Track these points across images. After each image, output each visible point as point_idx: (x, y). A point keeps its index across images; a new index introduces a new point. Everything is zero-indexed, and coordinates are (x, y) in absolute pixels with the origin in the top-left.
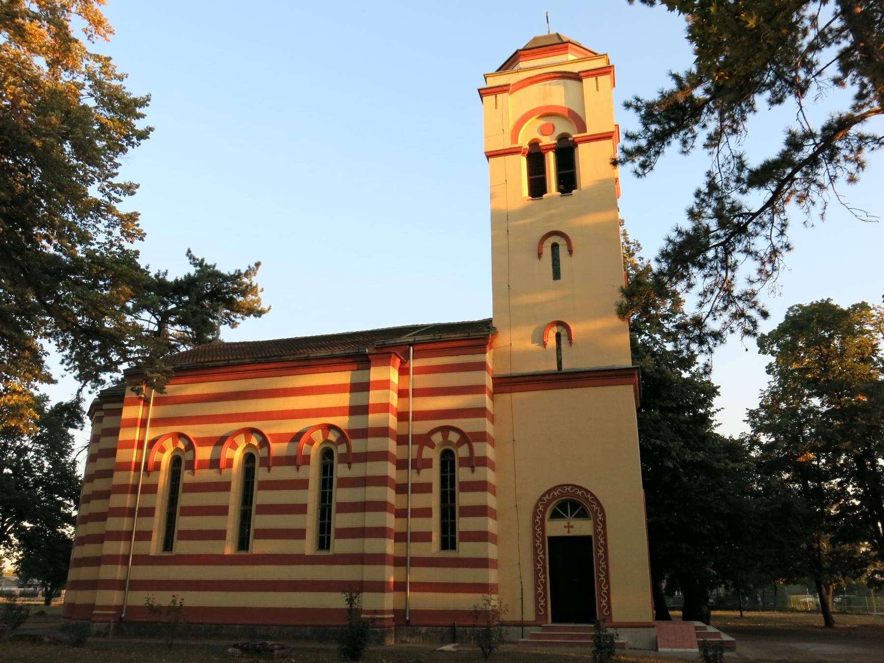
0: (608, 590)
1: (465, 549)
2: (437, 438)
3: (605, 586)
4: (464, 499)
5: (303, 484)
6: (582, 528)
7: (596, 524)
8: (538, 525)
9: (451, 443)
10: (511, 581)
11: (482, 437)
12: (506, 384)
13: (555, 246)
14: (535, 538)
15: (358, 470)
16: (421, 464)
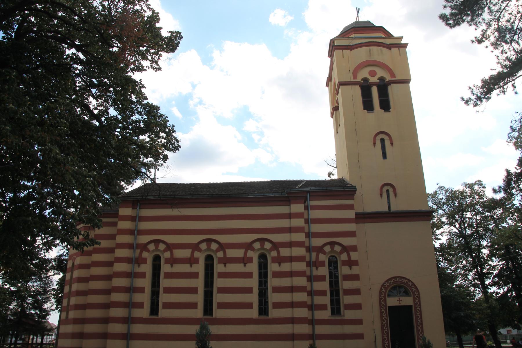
1: (349, 314)
3: (421, 333)
4: (346, 285)
5: (195, 275)
6: (407, 301)
8: (382, 300)
9: (336, 252)
11: (354, 248)
12: (363, 217)
13: (382, 140)
14: (381, 307)
15: (286, 267)
16: (317, 264)
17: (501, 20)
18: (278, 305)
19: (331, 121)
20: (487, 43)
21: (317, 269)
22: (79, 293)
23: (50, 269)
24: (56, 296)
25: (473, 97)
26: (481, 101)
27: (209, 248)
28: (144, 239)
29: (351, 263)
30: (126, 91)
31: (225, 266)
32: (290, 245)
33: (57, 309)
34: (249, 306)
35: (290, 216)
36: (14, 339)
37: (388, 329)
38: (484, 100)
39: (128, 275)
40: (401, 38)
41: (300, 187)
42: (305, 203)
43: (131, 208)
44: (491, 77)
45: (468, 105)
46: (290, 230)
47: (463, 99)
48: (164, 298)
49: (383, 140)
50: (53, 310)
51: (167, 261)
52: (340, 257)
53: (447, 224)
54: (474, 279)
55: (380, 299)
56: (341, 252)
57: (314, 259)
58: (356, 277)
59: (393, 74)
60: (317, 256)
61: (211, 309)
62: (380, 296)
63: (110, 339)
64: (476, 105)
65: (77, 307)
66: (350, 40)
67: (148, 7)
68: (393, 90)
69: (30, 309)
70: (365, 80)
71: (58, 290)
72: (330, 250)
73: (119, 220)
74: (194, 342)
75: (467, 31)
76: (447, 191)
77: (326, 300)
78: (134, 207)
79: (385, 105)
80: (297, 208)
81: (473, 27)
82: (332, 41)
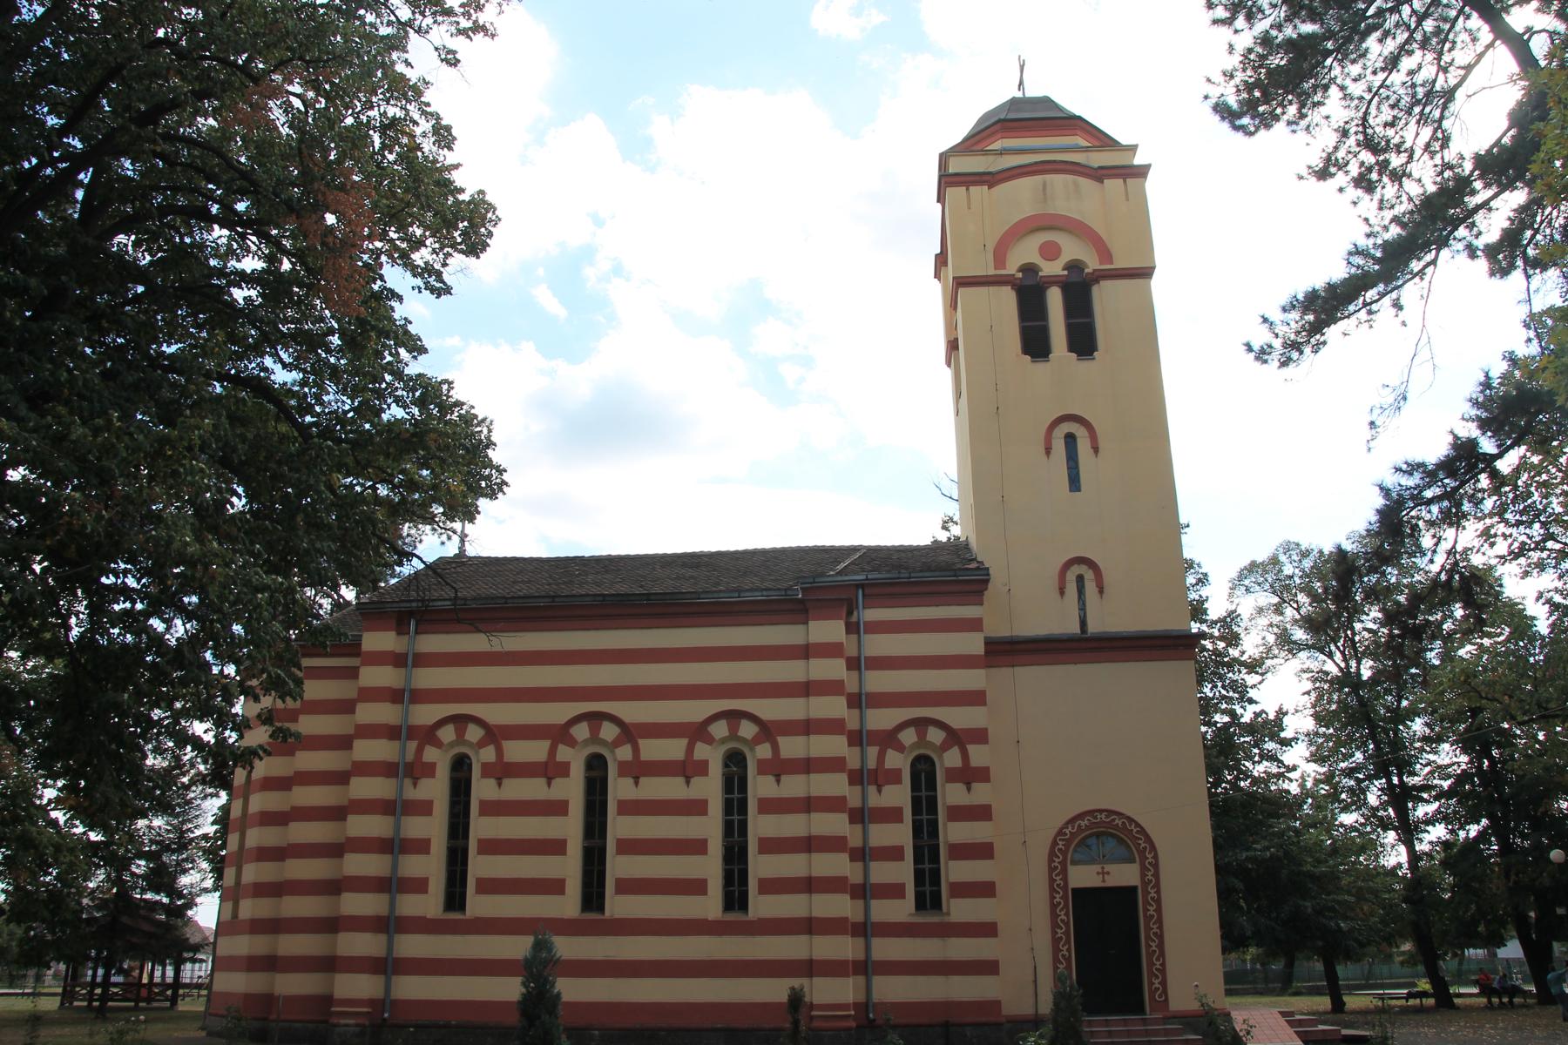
0: (1163, 965)
1: (960, 910)
2: (908, 737)
4: (953, 832)
6: (1124, 875)
7: (1144, 869)
9: (930, 745)
10: (1019, 959)
11: (980, 736)
13: (1070, 439)
14: (1052, 891)
15: (794, 786)
16: (881, 777)
17: (1371, 121)
18: (771, 886)
19: (948, 373)
20: (1341, 179)
21: (880, 791)
22: (266, 854)
23: (193, 782)
24: (212, 854)
25: (1277, 343)
26: (1301, 353)
27: (595, 737)
28: (426, 714)
29: (969, 775)
30: (374, 331)
31: (637, 783)
32: (807, 727)
33: (215, 890)
34: (697, 887)
35: (806, 652)
36: (100, 972)
37: (1069, 950)
38: (1307, 350)
39: (387, 807)
40: (1133, 149)
41: (840, 573)
42: (850, 613)
43: (393, 634)
44: (1331, 287)
45: (1265, 362)
46: (806, 689)
47: (1249, 348)
48: (479, 866)
49: (1071, 438)
50: (206, 890)
51: (487, 770)
52: (941, 757)
53: (1308, 647)
54: (1383, 805)
55: (1051, 869)
56: (945, 747)
57: (872, 763)
58: (982, 813)
59: (1105, 253)
60: (881, 758)
61: (602, 896)
62: (1051, 861)
63: (340, 972)
64: (1284, 364)
65: (262, 890)
66: (991, 158)
67: (424, 113)
68: (1105, 298)
69: (144, 891)
70: (1030, 269)
71: (217, 839)
72: (915, 739)
73: (364, 664)
74: (519, 979)
75: (1288, 146)
76: (1305, 554)
77: (903, 872)
78: (401, 629)
79: (1083, 342)
80: (828, 630)
81: (1301, 135)
82: (944, 158)
